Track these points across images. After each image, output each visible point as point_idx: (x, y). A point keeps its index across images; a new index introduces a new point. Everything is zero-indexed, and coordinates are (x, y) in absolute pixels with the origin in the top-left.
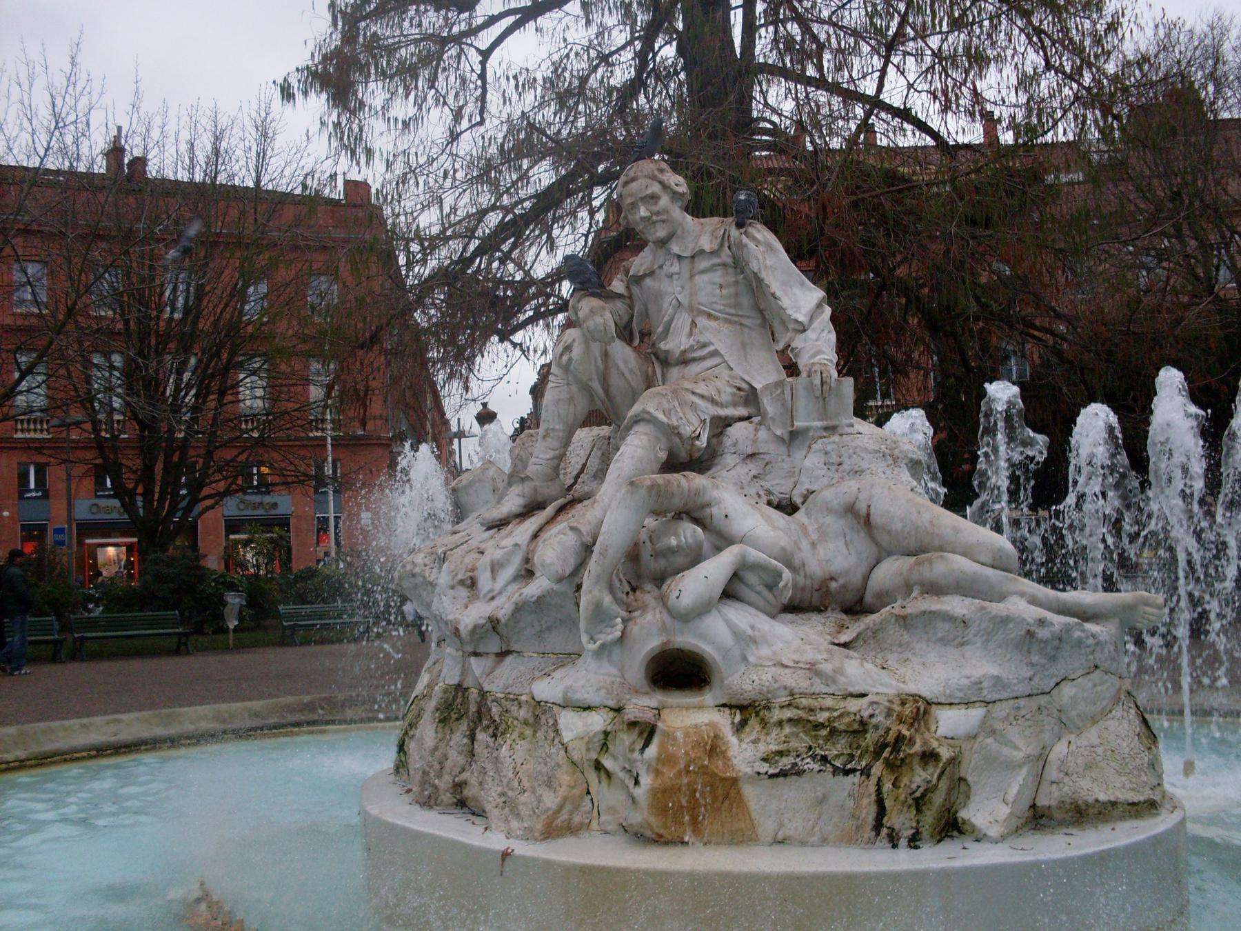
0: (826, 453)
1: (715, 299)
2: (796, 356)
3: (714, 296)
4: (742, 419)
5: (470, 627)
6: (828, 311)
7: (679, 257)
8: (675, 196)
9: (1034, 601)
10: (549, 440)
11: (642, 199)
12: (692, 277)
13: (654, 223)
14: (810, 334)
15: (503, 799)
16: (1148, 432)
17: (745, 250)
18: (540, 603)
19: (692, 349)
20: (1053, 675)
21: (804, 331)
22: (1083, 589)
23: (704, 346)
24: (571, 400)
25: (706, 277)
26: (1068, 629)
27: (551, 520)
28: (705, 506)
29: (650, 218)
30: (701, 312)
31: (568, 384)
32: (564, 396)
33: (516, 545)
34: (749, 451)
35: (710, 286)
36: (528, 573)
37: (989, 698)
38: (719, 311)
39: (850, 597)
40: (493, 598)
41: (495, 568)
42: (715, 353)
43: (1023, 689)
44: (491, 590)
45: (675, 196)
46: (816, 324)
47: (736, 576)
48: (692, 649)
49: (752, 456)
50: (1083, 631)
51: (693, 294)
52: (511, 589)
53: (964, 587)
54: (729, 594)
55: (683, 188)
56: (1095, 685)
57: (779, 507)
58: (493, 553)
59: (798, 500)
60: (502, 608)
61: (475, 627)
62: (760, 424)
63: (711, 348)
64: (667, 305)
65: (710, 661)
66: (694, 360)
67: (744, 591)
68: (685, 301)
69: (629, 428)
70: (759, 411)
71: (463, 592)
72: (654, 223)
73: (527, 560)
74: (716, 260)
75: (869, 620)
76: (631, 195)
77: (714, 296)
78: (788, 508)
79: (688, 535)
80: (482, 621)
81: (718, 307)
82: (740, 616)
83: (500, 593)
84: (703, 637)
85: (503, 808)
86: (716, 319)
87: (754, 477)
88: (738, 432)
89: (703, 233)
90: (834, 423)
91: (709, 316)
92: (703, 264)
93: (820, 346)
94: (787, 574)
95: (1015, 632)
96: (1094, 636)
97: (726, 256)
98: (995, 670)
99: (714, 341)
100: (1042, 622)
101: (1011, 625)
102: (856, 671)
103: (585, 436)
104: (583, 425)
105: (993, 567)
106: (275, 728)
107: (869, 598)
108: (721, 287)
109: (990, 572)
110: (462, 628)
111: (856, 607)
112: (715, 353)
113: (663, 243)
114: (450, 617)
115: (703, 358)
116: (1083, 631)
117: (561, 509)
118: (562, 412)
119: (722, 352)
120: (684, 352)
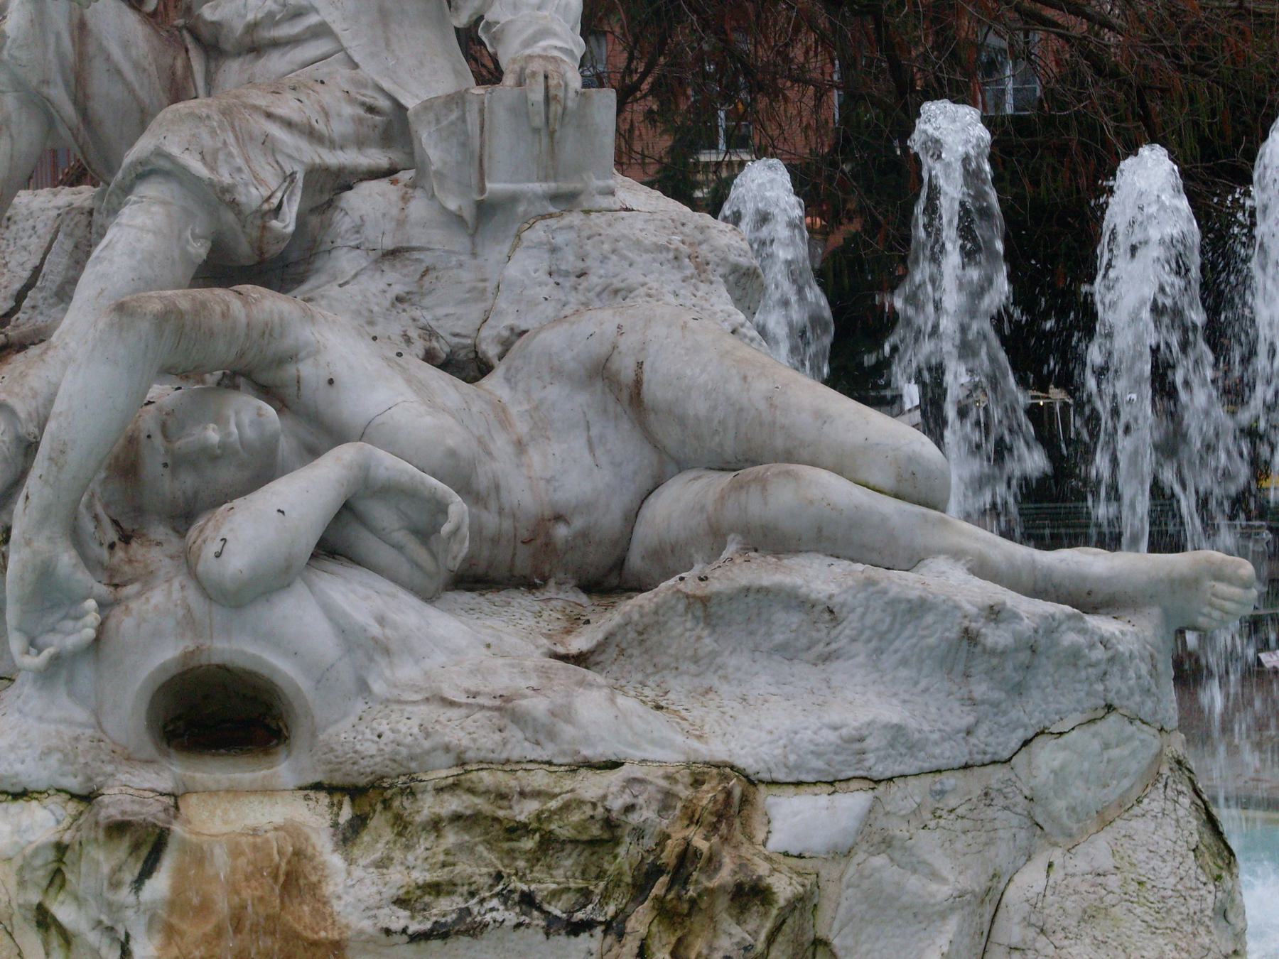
23: (298, 13)
26: (1050, 627)
37: (879, 771)
42: (322, 31)
47: (348, 511)
49: (393, 254)
50: (1083, 631)
56: (1106, 746)
62: (414, 185)
63: (313, 19)
66: (276, 44)
67: (367, 543)
69: (127, 190)
70: (413, 160)
82: (356, 596)
84: (272, 638)
88: (367, 201)
94: (458, 507)
95: (940, 633)
96: (1105, 643)
98: (892, 713)
100: (994, 613)
101: (930, 618)
105: (897, 496)
109: (889, 506)
112: (322, 31)
115: (294, 41)
116: (1083, 631)
119: (336, 28)
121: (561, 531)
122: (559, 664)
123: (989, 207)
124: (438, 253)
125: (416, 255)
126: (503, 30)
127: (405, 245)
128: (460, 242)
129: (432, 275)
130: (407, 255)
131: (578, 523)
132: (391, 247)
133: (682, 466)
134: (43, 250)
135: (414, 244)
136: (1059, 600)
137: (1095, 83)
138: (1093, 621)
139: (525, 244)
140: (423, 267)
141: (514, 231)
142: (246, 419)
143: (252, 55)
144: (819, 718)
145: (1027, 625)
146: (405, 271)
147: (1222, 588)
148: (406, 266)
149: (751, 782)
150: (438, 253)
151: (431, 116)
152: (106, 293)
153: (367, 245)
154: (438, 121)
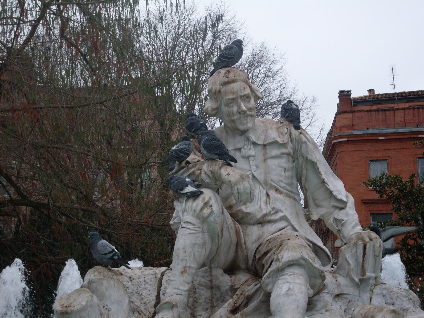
0: (384, 296)
1: (281, 178)
3: (281, 176)
7: (254, 144)
10: (186, 275)
11: (241, 97)
12: (265, 160)
13: (247, 116)
16: (63, 269)
17: (304, 146)
19: (269, 214)
24: (204, 244)
25: (276, 162)
30: (272, 187)
31: (203, 232)
32: (199, 241)
34: (337, 292)
38: (283, 188)
51: (267, 173)
63: (280, 214)
66: (270, 222)
68: (261, 178)
72: (247, 116)
74: (284, 151)
76: (233, 93)
77: (281, 176)
81: (283, 184)
86: (281, 193)
91: (277, 190)
92: (275, 152)
99: (283, 209)
108: (285, 170)
112: (284, 218)
115: (275, 221)
118: (197, 254)
119: (289, 217)
120: (265, 215)
124: (352, 296)
125: (345, 296)
126: (345, 223)
127: (342, 293)
128: (357, 293)
129: (351, 303)
130: (342, 296)
132: (338, 293)
135: (345, 292)
139: (375, 294)
140: (348, 300)
141: (368, 289)
143: (260, 225)
146: (343, 301)
148: (342, 300)
150: (352, 296)
151: (349, 250)
152: (299, 306)
153: (331, 292)
154: (351, 252)
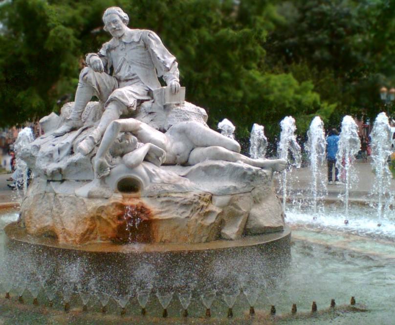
2: (166, 79)
4: (147, 100)
5: (51, 172)
6: (177, 64)
7: (125, 43)
8: (124, 21)
9: (246, 162)
14: (171, 72)
15: (63, 230)
18: (76, 164)
20: (252, 186)
21: (169, 70)
22: (366, 162)
23: (133, 75)
26: (257, 171)
27: (80, 134)
28: (137, 130)
29: (115, 29)
33: (68, 143)
34: (150, 111)
35: (134, 54)
36: (72, 153)
37: (233, 193)
39: (183, 161)
40: (59, 161)
41: (59, 151)
42: (137, 78)
43: (242, 190)
44: (58, 159)
45: (124, 21)
46: (173, 68)
47: (148, 154)
48: (129, 177)
49: (150, 113)
50: (262, 172)
52: (65, 158)
53: (225, 157)
54: (146, 159)
55: (127, 19)
56: (265, 189)
57: (160, 130)
58: (58, 145)
59: (166, 128)
60: (62, 165)
61: (53, 171)
62: (153, 102)
63: (135, 76)
64: (120, 59)
65: (128, 177)
67: (149, 159)
69: (108, 103)
70: (153, 98)
71: (48, 159)
73: (72, 148)
75: (189, 169)
78: (164, 131)
79: (132, 139)
80: (55, 170)
81: (138, 61)
82: (150, 167)
83: (61, 159)
84: (137, 173)
85: (64, 233)
87: (152, 120)
88: (146, 105)
89: (136, 34)
90: (179, 102)
92: (134, 46)
93: (174, 79)
94: (165, 153)
95: (240, 172)
96: (265, 173)
97: (142, 44)
98: (234, 185)
100: (250, 169)
101: (239, 170)
102: (187, 183)
103: (91, 104)
104: (91, 101)
105: (233, 151)
106: (150, 56)
107: (190, 162)
109: (232, 153)
110: (47, 171)
111: (185, 164)
112: (137, 78)
113: (120, 38)
114: (43, 168)
116: (262, 172)
117: (83, 130)
120: (126, 77)
121: (178, 157)
122: (182, 178)
123: (126, 242)
131: (181, 155)
133: (197, 146)
134: (245, 222)
136: (258, 167)
137: (82, 295)
138: (263, 170)
142: (132, 139)
144: (347, 222)
145: (254, 170)
147: (281, 165)
149: (212, 195)
